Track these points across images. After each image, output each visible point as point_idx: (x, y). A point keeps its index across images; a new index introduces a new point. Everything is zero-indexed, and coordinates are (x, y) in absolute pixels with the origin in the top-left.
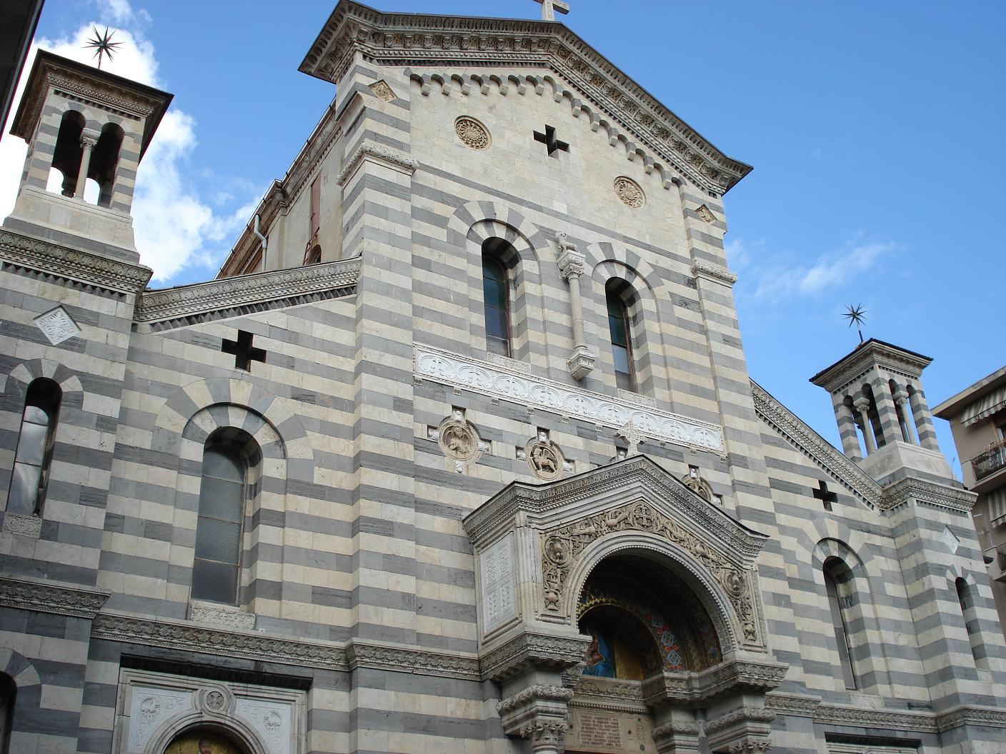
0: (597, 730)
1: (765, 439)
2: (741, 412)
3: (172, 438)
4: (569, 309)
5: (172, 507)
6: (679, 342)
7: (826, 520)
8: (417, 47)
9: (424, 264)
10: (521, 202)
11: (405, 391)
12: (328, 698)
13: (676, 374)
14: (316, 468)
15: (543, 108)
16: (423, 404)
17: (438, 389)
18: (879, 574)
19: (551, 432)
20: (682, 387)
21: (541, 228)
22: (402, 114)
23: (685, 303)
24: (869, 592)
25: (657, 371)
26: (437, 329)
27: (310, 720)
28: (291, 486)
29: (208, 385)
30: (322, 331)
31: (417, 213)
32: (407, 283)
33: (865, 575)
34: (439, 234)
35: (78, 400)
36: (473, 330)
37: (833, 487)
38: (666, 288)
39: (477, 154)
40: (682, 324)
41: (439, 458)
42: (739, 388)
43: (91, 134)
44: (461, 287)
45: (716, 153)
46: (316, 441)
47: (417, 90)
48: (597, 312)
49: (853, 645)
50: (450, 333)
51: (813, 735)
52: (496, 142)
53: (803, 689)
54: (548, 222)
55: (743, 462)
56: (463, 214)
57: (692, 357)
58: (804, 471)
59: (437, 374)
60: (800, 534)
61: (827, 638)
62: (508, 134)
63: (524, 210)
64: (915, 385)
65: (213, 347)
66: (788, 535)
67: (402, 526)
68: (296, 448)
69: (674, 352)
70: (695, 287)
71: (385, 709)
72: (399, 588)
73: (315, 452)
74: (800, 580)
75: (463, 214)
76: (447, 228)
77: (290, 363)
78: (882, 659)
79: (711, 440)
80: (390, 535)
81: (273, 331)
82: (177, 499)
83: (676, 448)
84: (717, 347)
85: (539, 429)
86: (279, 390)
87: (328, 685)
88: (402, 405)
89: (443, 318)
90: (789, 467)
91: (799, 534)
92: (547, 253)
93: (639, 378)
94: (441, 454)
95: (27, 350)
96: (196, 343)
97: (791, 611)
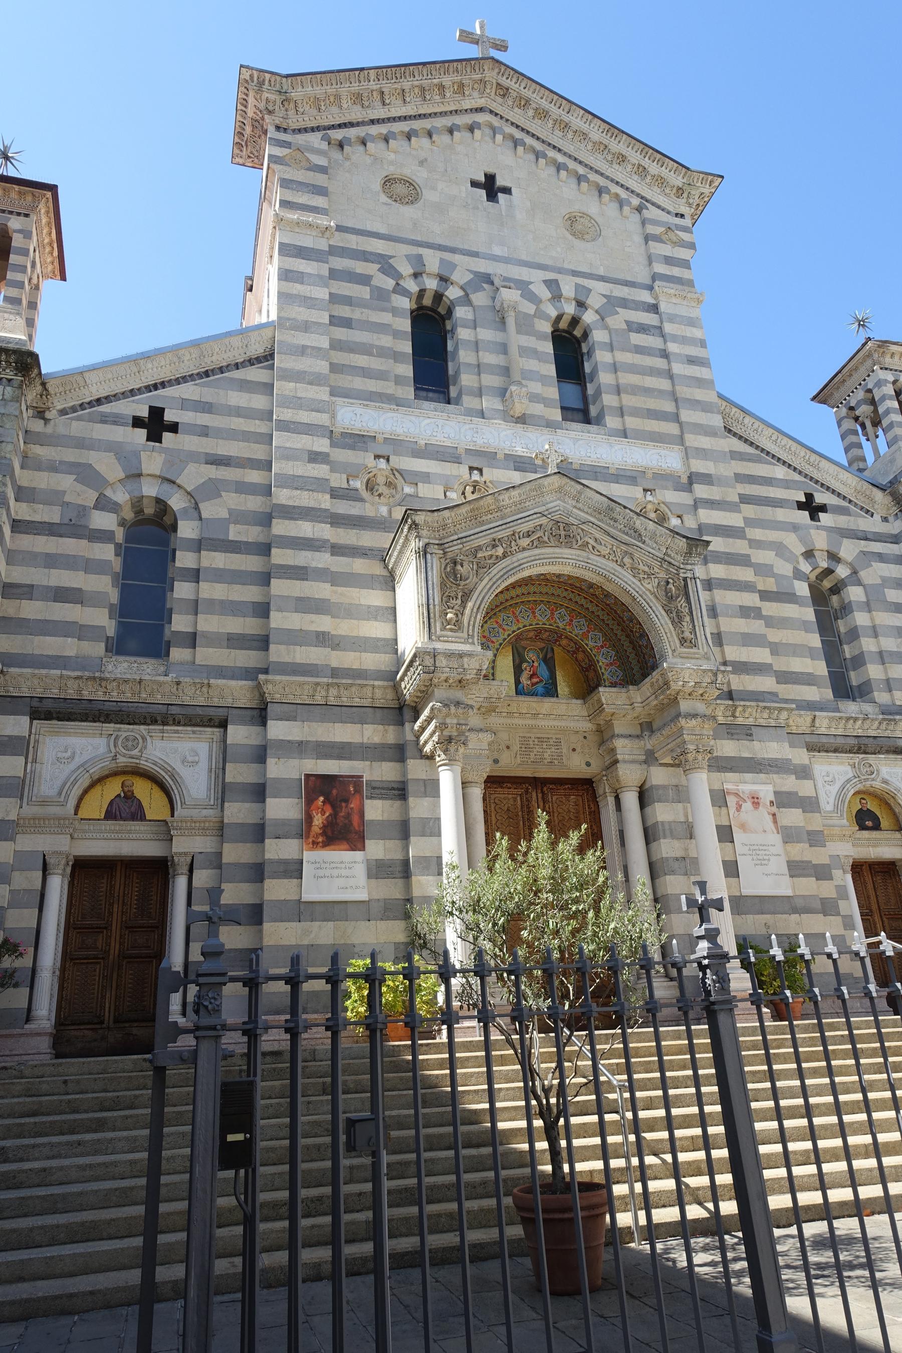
0: (537, 749)
1: (735, 455)
2: (709, 432)
3: (83, 511)
4: (504, 349)
5: (82, 573)
6: (634, 369)
7: (813, 532)
9: (347, 323)
10: (453, 250)
11: (322, 445)
13: (628, 400)
14: (232, 526)
15: (484, 154)
17: (357, 440)
18: (879, 581)
19: (485, 470)
20: (636, 412)
21: (476, 274)
22: (320, 179)
23: (642, 329)
24: (864, 599)
25: (608, 400)
26: (359, 383)
27: (224, 754)
28: (198, 545)
29: (118, 459)
30: (237, 398)
31: (334, 274)
32: (324, 343)
33: (859, 583)
34: (364, 292)
36: (399, 380)
37: (820, 498)
38: (619, 319)
39: (408, 211)
40: (639, 350)
41: (358, 504)
42: (706, 407)
44: (386, 341)
46: (232, 500)
47: (336, 155)
48: (540, 349)
49: (848, 656)
50: (372, 385)
51: (786, 745)
52: (428, 195)
53: (775, 699)
54: (483, 266)
55: (707, 479)
56: (388, 269)
57: (651, 382)
58: (787, 484)
59: (358, 425)
60: (785, 548)
61: (811, 649)
62: (440, 186)
63: (457, 258)
65: (123, 424)
66: (764, 549)
67: (316, 570)
68: (209, 510)
69: (626, 379)
70: (657, 313)
71: (297, 739)
72: (313, 628)
73: (231, 511)
74: (777, 593)
75: (388, 269)
76: (370, 285)
77: (204, 432)
78: (881, 667)
79: (669, 460)
80: (303, 580)
81: (185, 405)
82: (90, 566)
83: (629, 474)
84: (678, 368)
85: (471, 469)
86: (193, 457)
87: (243, 722)
88: (315, 457)
89: (365, 373)
90: (768, 481)
91: (780, 549)
92: (480, 298)
93: (593, 411)
94: (362, 500)
96: (104, 422)
97: (328, 467)
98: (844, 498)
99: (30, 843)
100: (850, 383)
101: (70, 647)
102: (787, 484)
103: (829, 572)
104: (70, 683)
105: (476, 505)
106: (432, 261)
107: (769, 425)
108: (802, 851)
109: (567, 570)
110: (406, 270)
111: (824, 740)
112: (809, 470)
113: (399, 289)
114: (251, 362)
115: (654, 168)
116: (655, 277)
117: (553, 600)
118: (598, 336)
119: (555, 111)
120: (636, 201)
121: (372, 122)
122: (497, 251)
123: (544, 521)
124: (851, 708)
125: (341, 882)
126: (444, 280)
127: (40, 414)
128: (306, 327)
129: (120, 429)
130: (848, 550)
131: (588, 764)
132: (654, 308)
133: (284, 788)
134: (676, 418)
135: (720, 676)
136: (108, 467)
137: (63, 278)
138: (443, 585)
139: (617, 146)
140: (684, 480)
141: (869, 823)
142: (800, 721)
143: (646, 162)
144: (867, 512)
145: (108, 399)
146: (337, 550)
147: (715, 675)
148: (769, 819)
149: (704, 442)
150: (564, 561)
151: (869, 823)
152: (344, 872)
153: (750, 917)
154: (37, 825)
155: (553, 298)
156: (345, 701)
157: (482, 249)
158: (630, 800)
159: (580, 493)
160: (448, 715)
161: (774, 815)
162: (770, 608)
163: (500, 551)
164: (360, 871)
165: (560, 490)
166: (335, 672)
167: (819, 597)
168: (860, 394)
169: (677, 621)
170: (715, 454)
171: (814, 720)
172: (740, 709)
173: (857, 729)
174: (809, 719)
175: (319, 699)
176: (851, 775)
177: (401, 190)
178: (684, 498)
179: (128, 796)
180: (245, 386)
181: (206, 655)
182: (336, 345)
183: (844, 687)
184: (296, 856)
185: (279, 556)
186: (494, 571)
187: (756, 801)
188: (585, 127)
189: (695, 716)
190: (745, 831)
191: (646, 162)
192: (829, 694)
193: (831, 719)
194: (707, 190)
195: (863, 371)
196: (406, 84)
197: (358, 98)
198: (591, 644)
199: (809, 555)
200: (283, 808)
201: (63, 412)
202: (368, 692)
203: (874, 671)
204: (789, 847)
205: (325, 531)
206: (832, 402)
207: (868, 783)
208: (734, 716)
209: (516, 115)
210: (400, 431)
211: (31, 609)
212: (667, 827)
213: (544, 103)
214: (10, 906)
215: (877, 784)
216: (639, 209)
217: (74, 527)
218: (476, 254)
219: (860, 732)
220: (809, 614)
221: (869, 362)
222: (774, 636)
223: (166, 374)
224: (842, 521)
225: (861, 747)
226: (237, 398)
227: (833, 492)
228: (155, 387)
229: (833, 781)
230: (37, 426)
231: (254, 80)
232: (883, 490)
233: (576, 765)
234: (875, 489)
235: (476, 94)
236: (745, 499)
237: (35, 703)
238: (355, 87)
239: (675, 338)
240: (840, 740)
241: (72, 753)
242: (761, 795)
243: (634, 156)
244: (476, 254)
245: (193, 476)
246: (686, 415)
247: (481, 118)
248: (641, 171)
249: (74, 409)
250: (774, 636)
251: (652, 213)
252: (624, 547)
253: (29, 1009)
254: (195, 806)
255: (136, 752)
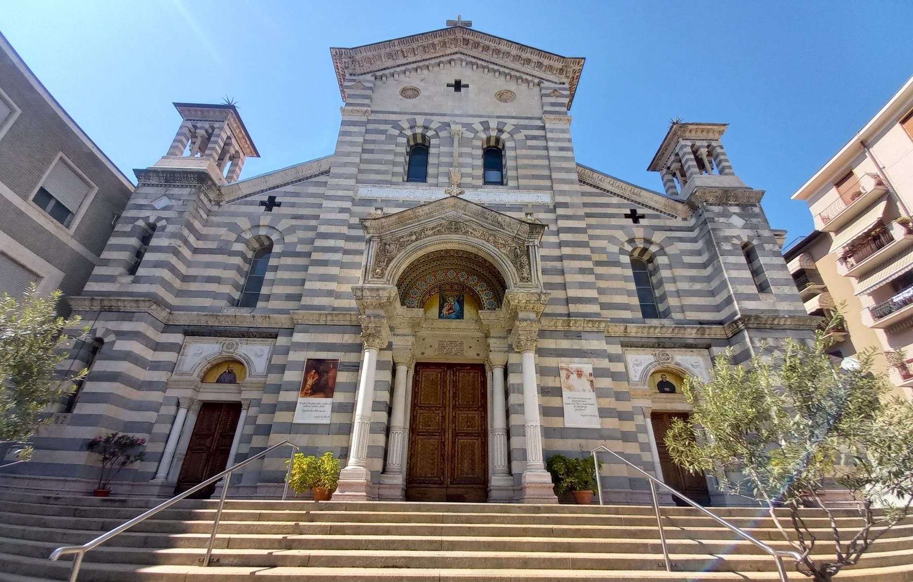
1: (584, 194)
3: (228, 243)
4: (451, 154)
8: (379, 63)
9: (371, 151)
11: (348, 204)
12: (281, 341)
16: (356, 209)
20: (526, 177)
26: (373, 177)
27: (275, 351)
28: (279, 255)
30: (312, 190)
33: (665, 254)
34: (383, 137)
35: (163, 228)
37: (640, 211)
39: (414, 101)
42: (568, 170)
43: (200, 132)
45: (434, 33)
46: (301, 234)
50: (379, 177)
52: (423, 93)
54: (446, 119)
55: (565, 205)
58: (619, 206)
60: (615, 238)
63: (434, 118)
64: (714, 144)
68: (288, 239)
69: (521, 162)
77: (293, 205)
79: (545, 198)
81: (286, 194)
84: (552, 153)
86: (286, 216)
88: (342, 210)
89: (377, 172)
92: (443, 134)
95: (144, 213)
98: (657, 210)
99: (172, 393)
100: (667, 154)
101: (207, 302)
102: (619, 206)
103: (645, 250)
104: (203, 318)
105: (402, 215)
106: (420, 120)
107: (607, 176)
108: (610, 403)
109: (456, 247)
110: (406, 125)
111: (633, 340)
112: (634, 197)
113: (401, 134)
114: (322, 174)
115: (546, 62)
116: (545, 112)
117: (457, 267)
118: (509, 144)
119: (492, 45)
120: (536, 80)
121: (398, 66)
122: (457, 112)
123: (443, 222)
124: (655, 322)
125: (316, 414)
126: (426, 128)
127: (218, 204)
128: (349, 154)
129: (253, 207)
130: (658, 237)
131: (478, 355)
132: (543, 128)
133: (294, 366)
134: (550, 177)
135: (543, 297)
136: (244, 223)
137: (258, 156)
138: (377, 255)
139: (525, 55)
140: (552, 207)
141: (667, 389)
142: (616, 329)
143: (542, 60)
144: (673, 216)
145: (250, 195)
146: (346, 252)
147: (540, 295)
148: (588, 384)
149: (566, 187)
150: (453, 242)
151: (667, 389)
152: (319, 409)
153: (569, 441)
154: (177, 385)
155: (485, 129)
156: (336, 323)
157: (449, 112)
158: (498, 373)
159: (466, 206)
160: (370, 322)
161: (592, 381)
162: (599, 270)
163: (414, 237)
164: (329, 408)
165: (454, 206)
166: (334, 309)
167: (636, 264)
168: (673, 158)
169: (520, 267)
170: (572, 193)
171: (626, 328)
172: (572, 322)
173: (657, 333)
174: (622, 328)
175: (322, 322)
176: (653, 360)
177: (410, 93)
178: (552, 216)
179: (230, 372)
180: (318, 184)
181: (273, 304)
182: (363, 161)
183: (650, 309)
184: (294, 400)
185: (315, 256)
186: (408, 247)
187: (580, 374)
188: (508, 49)
189: (526, 320)
190: (571, 390)
191: (542, 60)
192: (639, 315)
193: (638, 328)
194: (577, 67)
195: (673, 145)
196: (415, 45)
197: (390, 56)
198: (479, 289)
199: (631, 241)
200: (294, 376)
201: (228, 202)
202: (348, 317)
203: (672, 302)
204: (601, 400)
205: (341, 243)
206: (658, 168)
207: (665, 365)
208: (569, 326)
209: (474, 53)
210: (390, 196)
211: (193, 287)
212: (516, 387)
213: (487, 43)
214: (156, 422)
215: (672, 365)
216: (539, 85)
217: (224, 250)
218: (445, 115)
219: (659, 335)
220: (629, 272)
221: (676, 137)
222: (602, 284)
223: (279, 182)
224: (655, 222)
225: (660, 344)
226: (312, 190)
227: (650, 207)
228: (274, 188)
229: (640, 364)
230: (215, 208)
231: (338, 54)
232: (682, 202)
233: (470, 355)
234: (677, 203)
235: (453, 46)
236: (588, 215)
237: (186, 328)
238: (388, 50)
239: (552, 140)
240: (644, 340)
241: (205, 350)
242: (584, 370)
243: (535, 58)
244: (445, 115)
245: (283, 225)
246: (555, 175)
247: (455, 57)
248: (539, 65)
249: (234, 200)
250: (602, 284)
251: (546, 84)
252: (490, 232)
253: (156, 473)
254: (256, 376)
255: (232, 350)
